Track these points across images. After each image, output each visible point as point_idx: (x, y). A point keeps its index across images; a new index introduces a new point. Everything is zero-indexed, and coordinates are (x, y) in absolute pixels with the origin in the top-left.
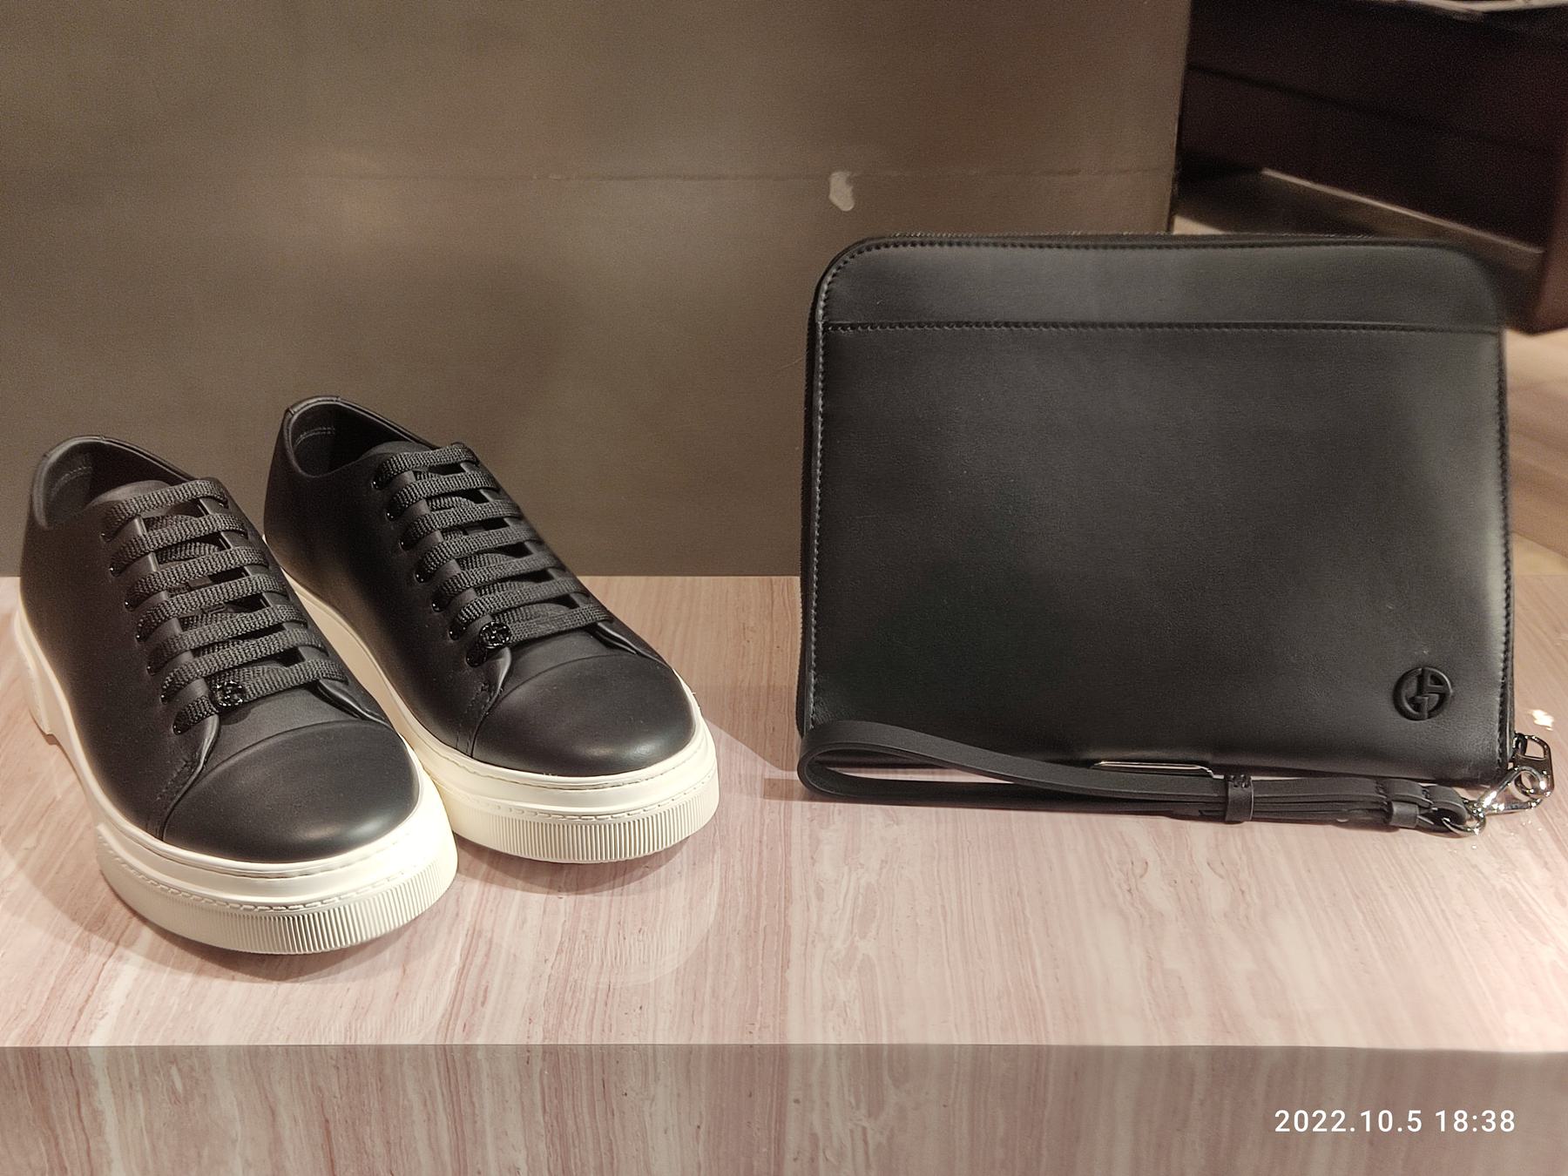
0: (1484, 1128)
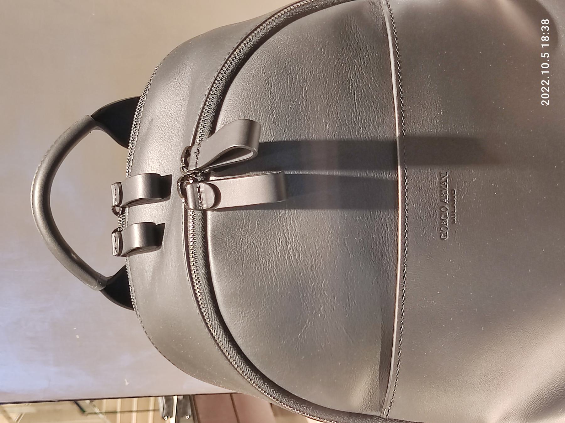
0: (548, 30)
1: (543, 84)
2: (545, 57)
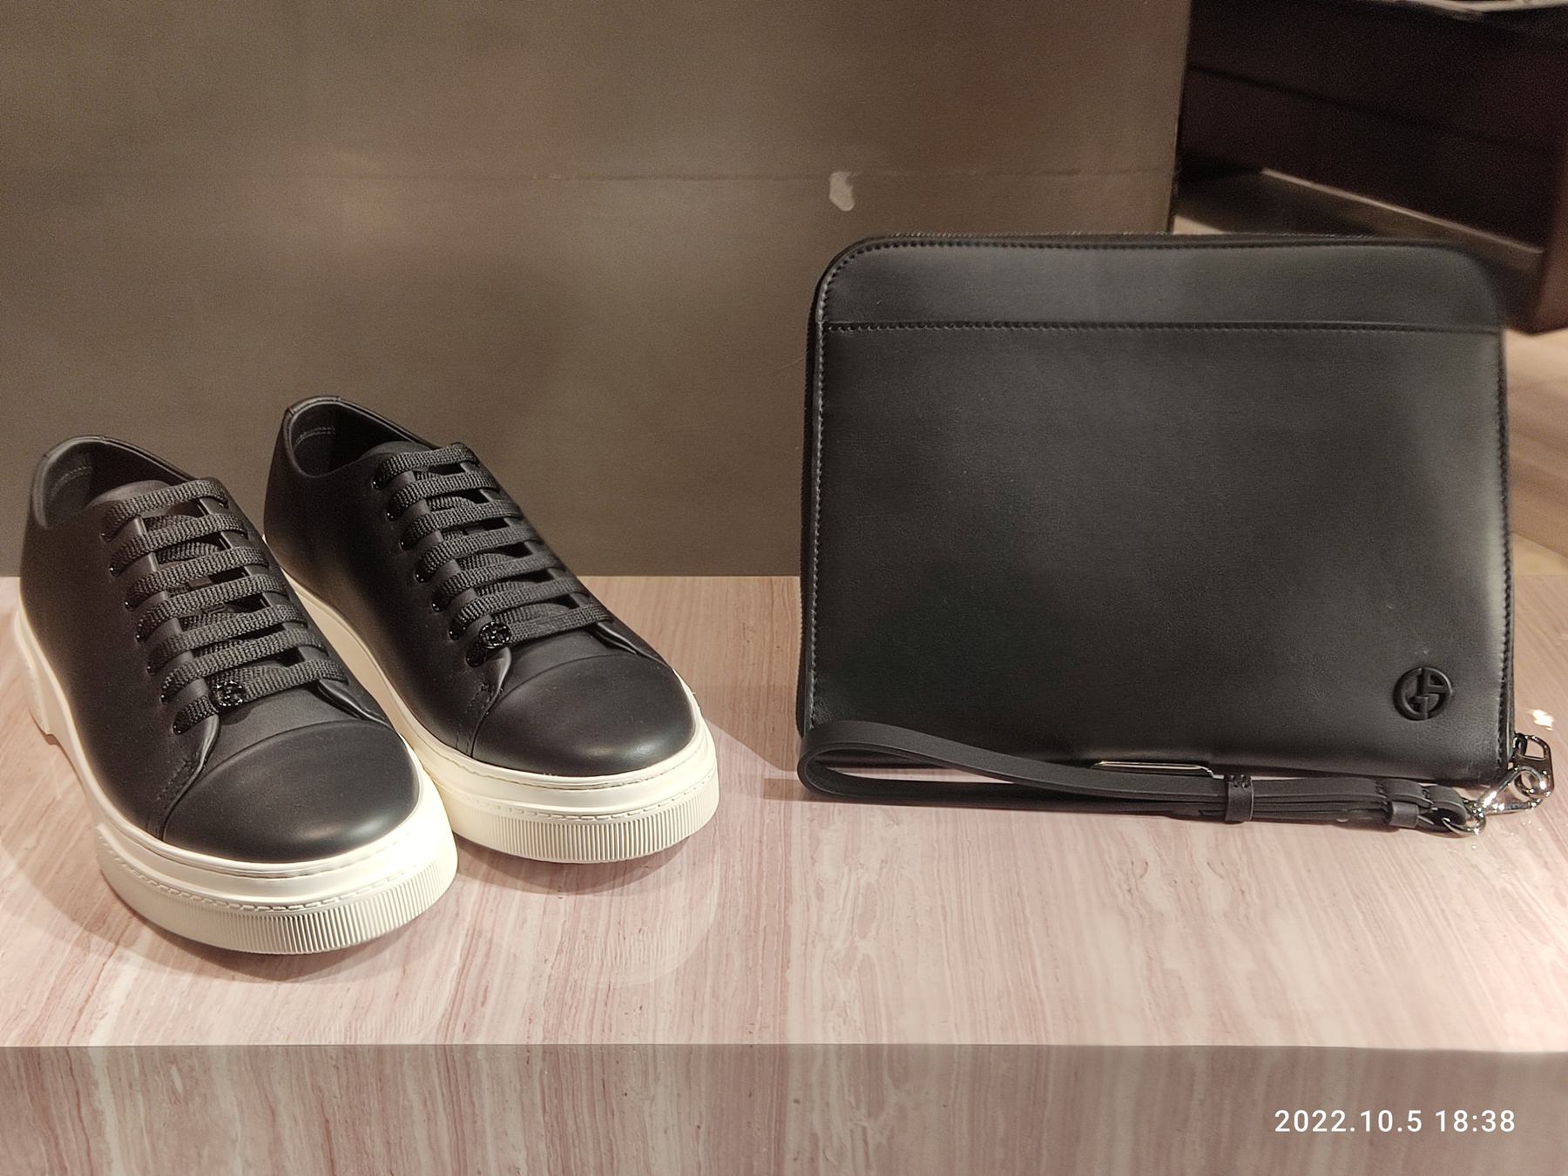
0: (1484, 1128)
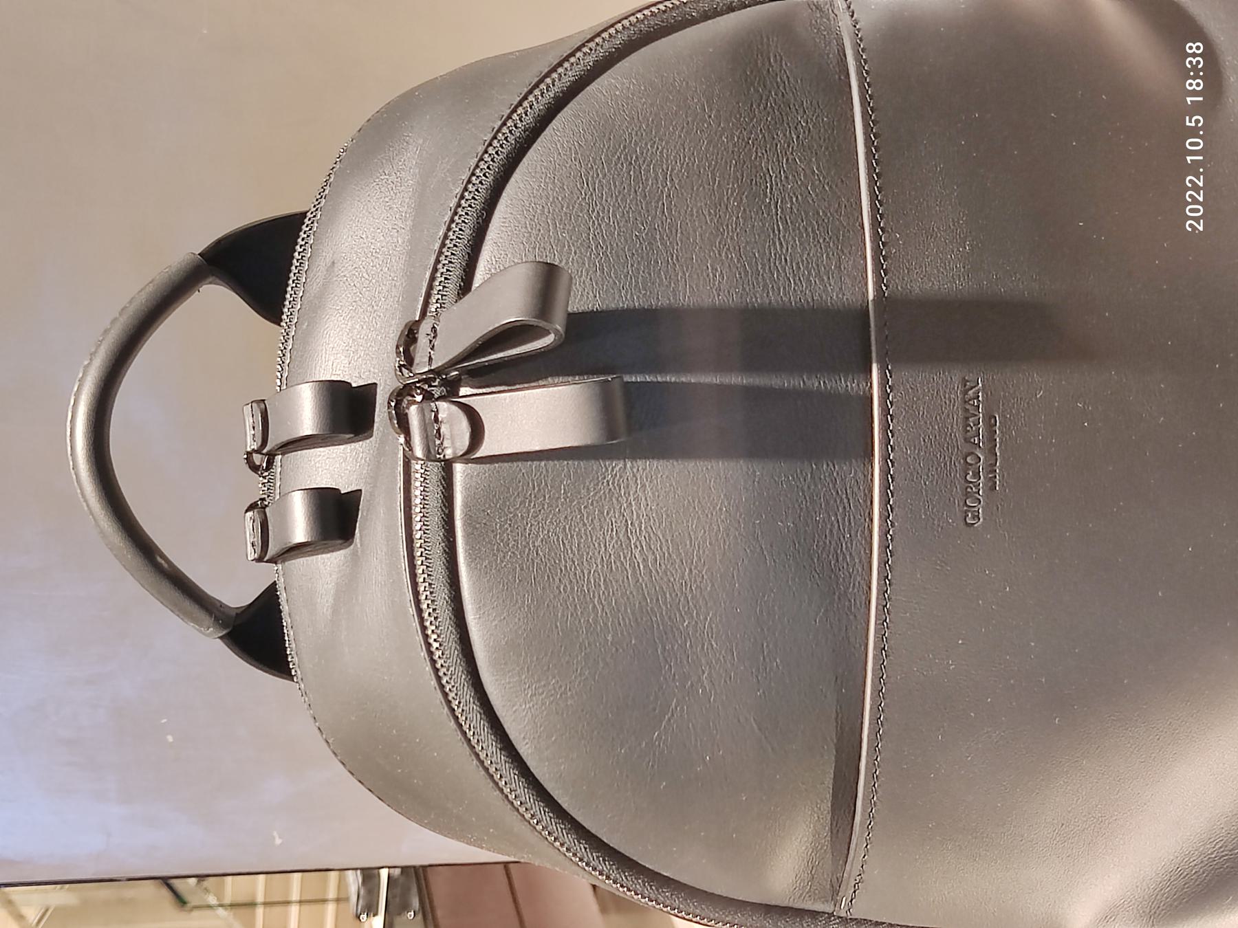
0: (1200, 66)
1: (1190, 185)
2: (1193, 124)
